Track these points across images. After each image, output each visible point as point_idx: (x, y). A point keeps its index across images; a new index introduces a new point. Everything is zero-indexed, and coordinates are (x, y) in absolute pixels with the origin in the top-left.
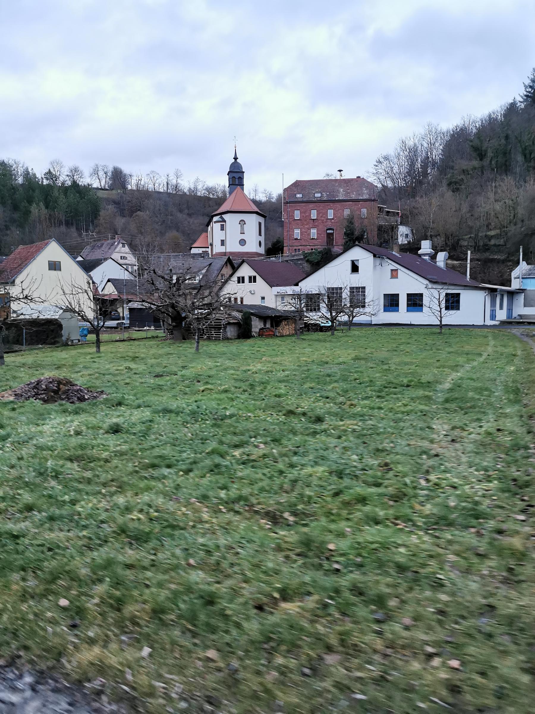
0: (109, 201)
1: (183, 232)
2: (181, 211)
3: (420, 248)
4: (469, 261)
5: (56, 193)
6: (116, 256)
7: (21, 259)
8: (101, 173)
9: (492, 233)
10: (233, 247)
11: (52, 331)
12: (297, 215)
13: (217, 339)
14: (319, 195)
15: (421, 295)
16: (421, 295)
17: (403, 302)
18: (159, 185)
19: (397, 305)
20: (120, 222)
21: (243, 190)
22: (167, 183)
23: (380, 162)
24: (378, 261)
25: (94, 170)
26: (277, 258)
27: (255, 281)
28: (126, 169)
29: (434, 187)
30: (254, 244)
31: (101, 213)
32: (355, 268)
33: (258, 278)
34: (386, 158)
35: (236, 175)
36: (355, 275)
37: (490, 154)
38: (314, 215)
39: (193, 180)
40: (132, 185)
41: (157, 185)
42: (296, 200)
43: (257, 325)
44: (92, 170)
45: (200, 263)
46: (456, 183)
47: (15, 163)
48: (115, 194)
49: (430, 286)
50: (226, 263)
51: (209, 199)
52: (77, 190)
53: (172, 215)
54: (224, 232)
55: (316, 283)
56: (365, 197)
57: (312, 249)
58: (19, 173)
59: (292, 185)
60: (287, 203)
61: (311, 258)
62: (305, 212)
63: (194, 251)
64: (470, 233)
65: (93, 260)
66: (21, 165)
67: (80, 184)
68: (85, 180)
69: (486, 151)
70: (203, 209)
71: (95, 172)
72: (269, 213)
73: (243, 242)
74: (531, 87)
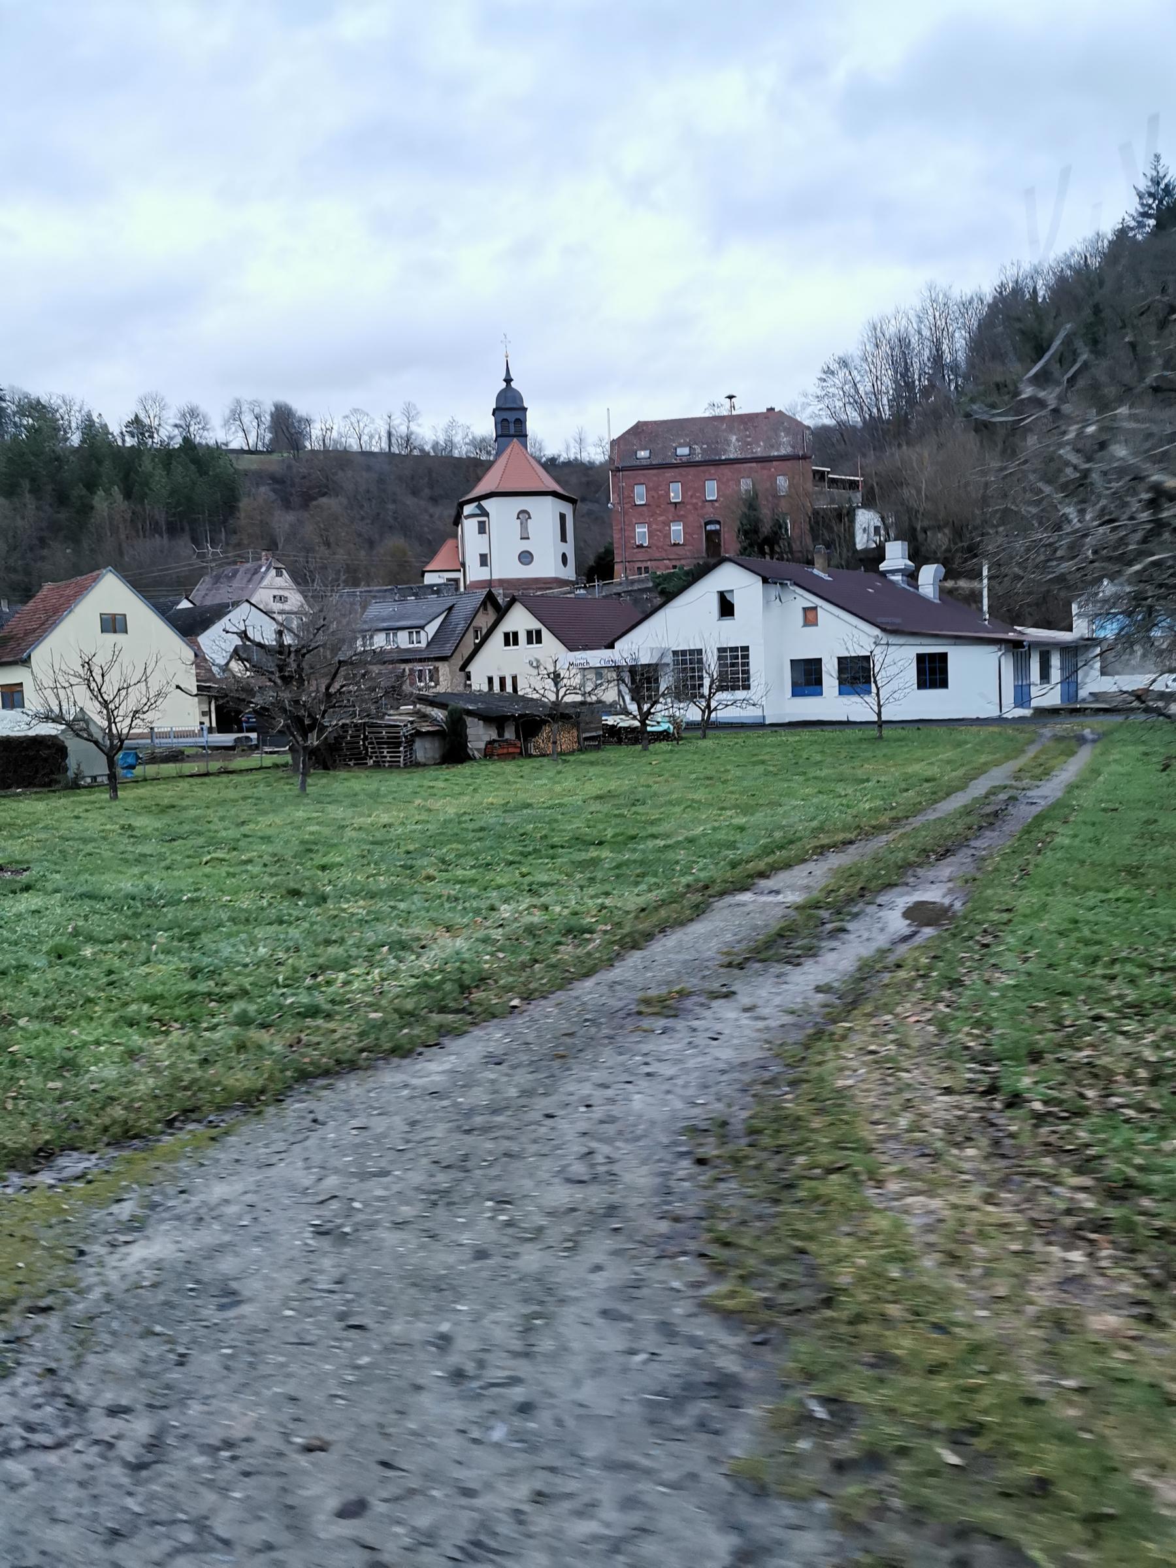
0: (259, 477)
2: (415, 493)
3: (883, 559)
5: (147, 465)
6: (263, 596)
8: (248, 419)
10: (506, 568)
11: (46, 760)
12: (640, 495)
13: (394, 765)
14: (686, 451)
17: (830, 672)
18: (371, 437)
19: (819, 682)
20: (282, 521)
22: (390, 434)
24: (774, 590)
25: (233, 412)
26: (605, 586)
27: (539, 641)
28: (300, 407)
30: (550, 559)
31: (241, 505)
32: (726, 608)
33: (546, 634)
34: (844, 363)
35: (510, 416)
36: (727, 623)
38: (676, 493)
39: (443, 422)
40: (314, 439)
41: (365, 438)
43: (478, 735)
44: (227, 413)
45: (435, 604)
48: (275, 463)
50: (484, 604)
52: (194, 456)
53: (394, 501)
54: (486, 536)
55: (645, 643)
58: (74, 425)
59: (628, 432)
62: (656, 489)
63: (429, 579)
66: (76, 408)
70: (428, 491)
71: (236, 415)
73: (526, 557)
74: (1151, 195)
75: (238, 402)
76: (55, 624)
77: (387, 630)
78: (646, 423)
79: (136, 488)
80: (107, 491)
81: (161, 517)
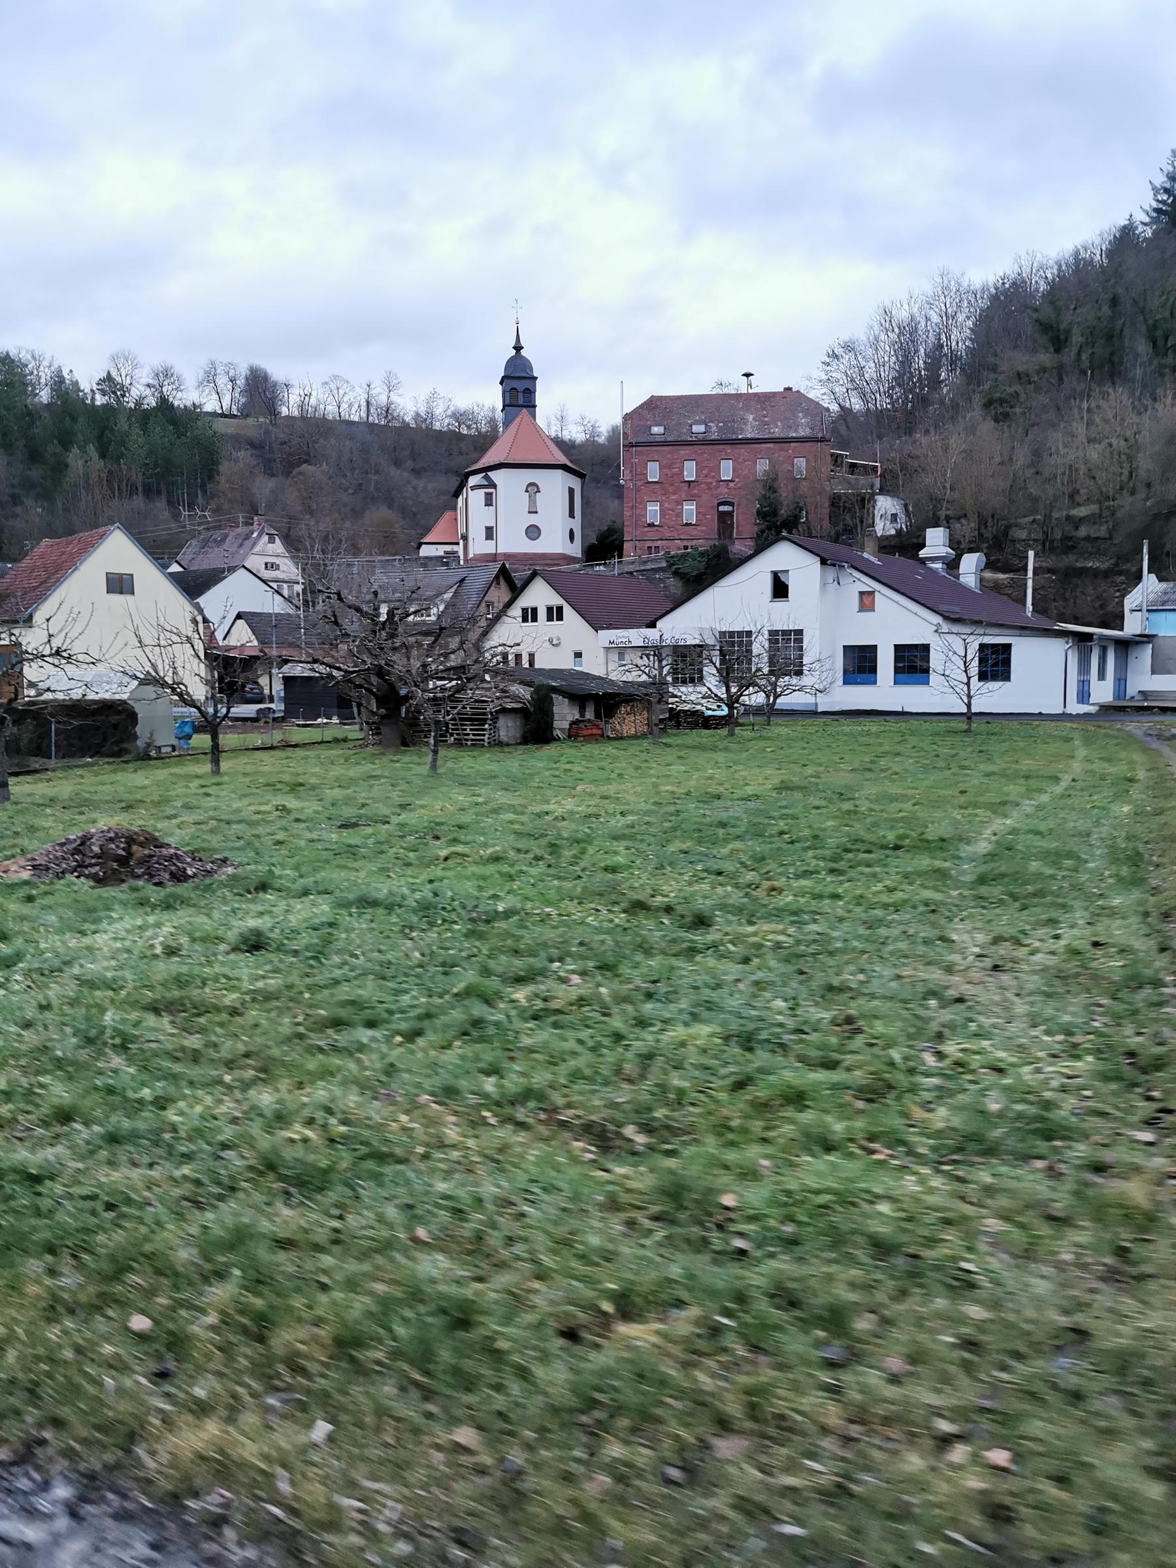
0: (239, 441)
1: (403, 511)
2: (397, 464)
3: (923, 546)
4: (1030, 574)
5: (123, 424)
6: (255, 562)
7: (46, 569)
8: (222, 381)
9: (1082, 512)
10: (512, 542)
11: (115, 727)
12: (653, 472)
13: (477, 745)
14: (702, 428)
15: (926, 648)
16: (926, 648)
17: (886, 663)
18: (351, 406)
19: (873, 670)
20: (264, 487)
21: (534, 417)
22: (368, 403)
23: (835, 356)
24: (831, 573)
25: (208, 373)
26: (609, 566)
27: (560, 618)
28: (277, 371)
29: (955, 410)
30: (558, 536)
31: (221, 468)
32: (780, 590)
33: (568, 611)
34: (849, 347)
35: (519, 385)
36: (780, 605)
37: (1077, 338)
38: (690, 471)
39: (423, 395)
40: (289, 407)
41: (344, 406)
42: (651, 439)
43: (564, 714)
44: (201, 374)
45: (441, 577)
46: (1002, 401)
47: (34, 357)
48: (252, 426)
49: (945, 627)
50: (497, 577)
51: (459, 437)
52: (168, 416)
53: (377, 472)
54: (492, 509)
55: (694, 621)
56: (803, 432)
57: (686, 548)
58: (43, 381)
59: (641, 407)
60: (631, 445)
61: (683, 567)
62: (670, 467)
63: (425, 551)
64: (1034, 511)
65: (205, 571)
66: (45, 363)
67: (176, 403)
68: (187, 396)
69: (1068, 331)
70: (446, 459)
71: (210, 378)
72: (592, 467)
73: (533, 532)
74: (1166, 191)
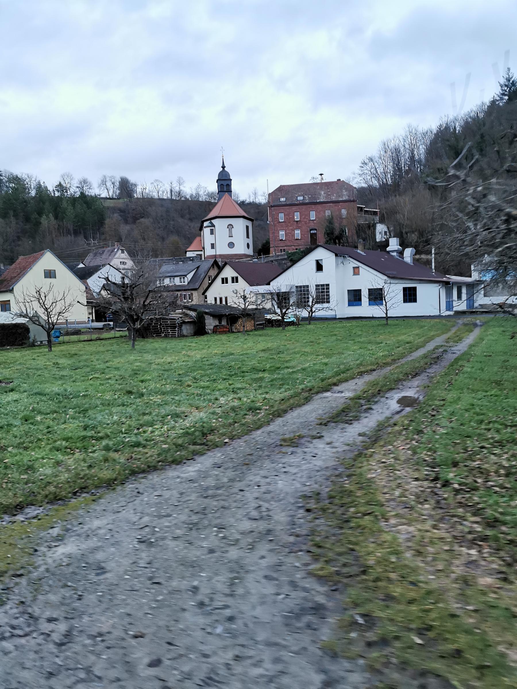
0: (114, 210)
2: (182, 216)
3: (388, 246)
5: (65, 204)
6: (116, 262)
8: (109, 184)
10: (222, 250)
11: (20, 334)
12: (281, 218)
13: (173, 336)
14: (301, 198)
17: (365, 295)
18: (163, 192)
19: (360, 300)
20: (124, 229)
22: (171, 191)
24: (340, 259)
25: (103, 181)
26: (266, 258)
27: (237, 282)
28: (132, 179)
30: (242, 246)
31: (106, 222)
32: (319, 267)
33: (240, 278)
34: (371, 159)
35: (224, 183)
36: (320, 274)
38: (297, 217)
39: (195, 186)
40: (138, 193)
41: (160, 192)
43: (210, 323)
44: (100, 181)
45: (191, 265)
48: (121, 203)
50: (213, 265)
52: (85, 201)
53: (173, 220)
54: (213, 236)
55: (284, 283)
58: (32, 187)
59: (276, 190)
62: (288, 215)
63: (189, 254)
66: (33, 179)
70: (188, 216)
71: (104, 182)
73: (231, 245)
74: (506, 86)
75: (105, 177)
76: (24, 274)
77: (170, 277)
78: (284, 186)
79: (60, 214)
80: (47, 216)
81: (71, 227)
